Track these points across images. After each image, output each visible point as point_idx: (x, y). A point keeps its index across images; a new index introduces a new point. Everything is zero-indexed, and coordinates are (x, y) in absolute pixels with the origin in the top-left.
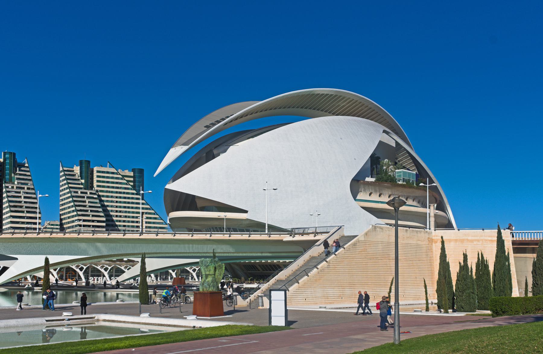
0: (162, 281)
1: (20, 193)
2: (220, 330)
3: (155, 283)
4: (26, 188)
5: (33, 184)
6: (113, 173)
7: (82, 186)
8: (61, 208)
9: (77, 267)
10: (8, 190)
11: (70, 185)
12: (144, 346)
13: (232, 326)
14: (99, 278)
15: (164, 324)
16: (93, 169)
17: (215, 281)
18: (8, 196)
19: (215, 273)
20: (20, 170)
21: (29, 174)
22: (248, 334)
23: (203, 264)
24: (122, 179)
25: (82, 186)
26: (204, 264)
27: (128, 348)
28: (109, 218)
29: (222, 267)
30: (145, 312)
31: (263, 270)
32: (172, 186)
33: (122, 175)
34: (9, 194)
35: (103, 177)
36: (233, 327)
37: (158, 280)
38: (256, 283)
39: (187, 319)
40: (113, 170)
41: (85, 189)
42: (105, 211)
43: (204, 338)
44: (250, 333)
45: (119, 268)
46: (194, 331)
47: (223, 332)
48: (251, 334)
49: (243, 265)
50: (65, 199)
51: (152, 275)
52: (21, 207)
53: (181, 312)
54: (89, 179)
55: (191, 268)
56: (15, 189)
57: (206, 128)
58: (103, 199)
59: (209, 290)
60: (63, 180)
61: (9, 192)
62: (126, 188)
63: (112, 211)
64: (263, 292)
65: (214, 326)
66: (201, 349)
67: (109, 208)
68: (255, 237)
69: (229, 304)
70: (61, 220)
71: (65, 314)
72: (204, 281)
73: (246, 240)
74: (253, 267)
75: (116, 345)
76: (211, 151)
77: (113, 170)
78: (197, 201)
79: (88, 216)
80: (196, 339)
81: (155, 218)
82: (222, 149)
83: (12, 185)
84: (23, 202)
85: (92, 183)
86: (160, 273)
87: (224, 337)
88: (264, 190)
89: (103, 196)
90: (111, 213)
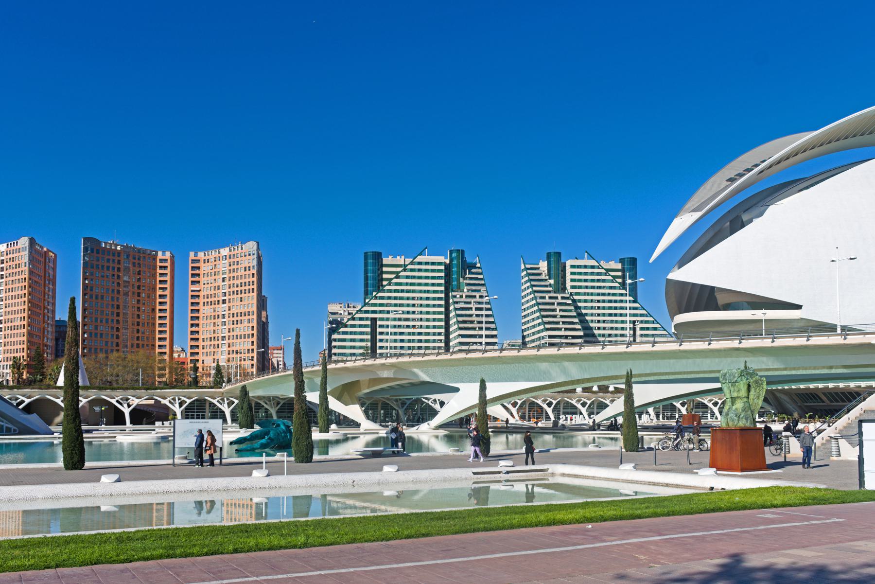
0: (666, 420)
1: (470, 303)
2: (761, 496)
3: (655, 422)
4: (478, 297)
5: (487, 290)
6: (593, 267)
7: (550, 289)
8: (523, 321)
9: (544, 401)
10: (455, 300)
11: (535, 289)
12: (611, 521)
13: (784, 489)
14: (574, 416)
15: (659, 483)
16: (565, 263)
17: (748, 408)
18: (456, 309)
19: (748, 395)
20: (470, 273)
21: (481, 276)
22: (819, 504)
23: (726, 380)
24: (605, 274)
25: (550, 289)
26: (728, 379)
27: (582, 522)
28: (588, 332)
29: (762, 384)
30: (629, 461)
31: (831, 402)
32: (679, 275)
33: (605, 269)
34: (456, 306)
35: (580, 274)
36: (786, 489)
37: (659, 420)
38: (820, 421)
39: (699, 474)
40: (593, 263)
41: (555, 292)
42: (583, 321)
43: (730, 509)
44: (823, 502)
45: (602, 402)
46: (710, 495)
47: (768, 498)
48: (824, 504)
49: (796, 394)
50: (528, 308)
51: (651, 410)
52: (472, 322)
53: (690, 464)
54: (560, 278)
55: (710, 400)
56: (464, 299)
57: (729, 183)
58: (579, 304)
59: (739, 425)
60: (526, 282)
61: (457, 303)
62: (611, 288)
63: (592, 321)
64: (837, 431)
65: (748, 487)
66: (723, 530)
67: (587, 318)
68: (818, 340)
69: (774, 452)
70: (524, 337)
71: (502, 463)
72: (729, 408)
73: (802, 346)
74: (813, 396)
75: (560, 516)
76: (738, 217)
77: (593, 263)
78: (718, 296)
79: (560, 329)
80: (713, 510)
81: (655, 329)
82: (756, 211)
83: (461, 294)
84: (474, 316)
85: (564, 283)
86: (663, 406)
87: (769, 508)
88: (833, 261)
89: (580, 301)
90: (592, 325)
